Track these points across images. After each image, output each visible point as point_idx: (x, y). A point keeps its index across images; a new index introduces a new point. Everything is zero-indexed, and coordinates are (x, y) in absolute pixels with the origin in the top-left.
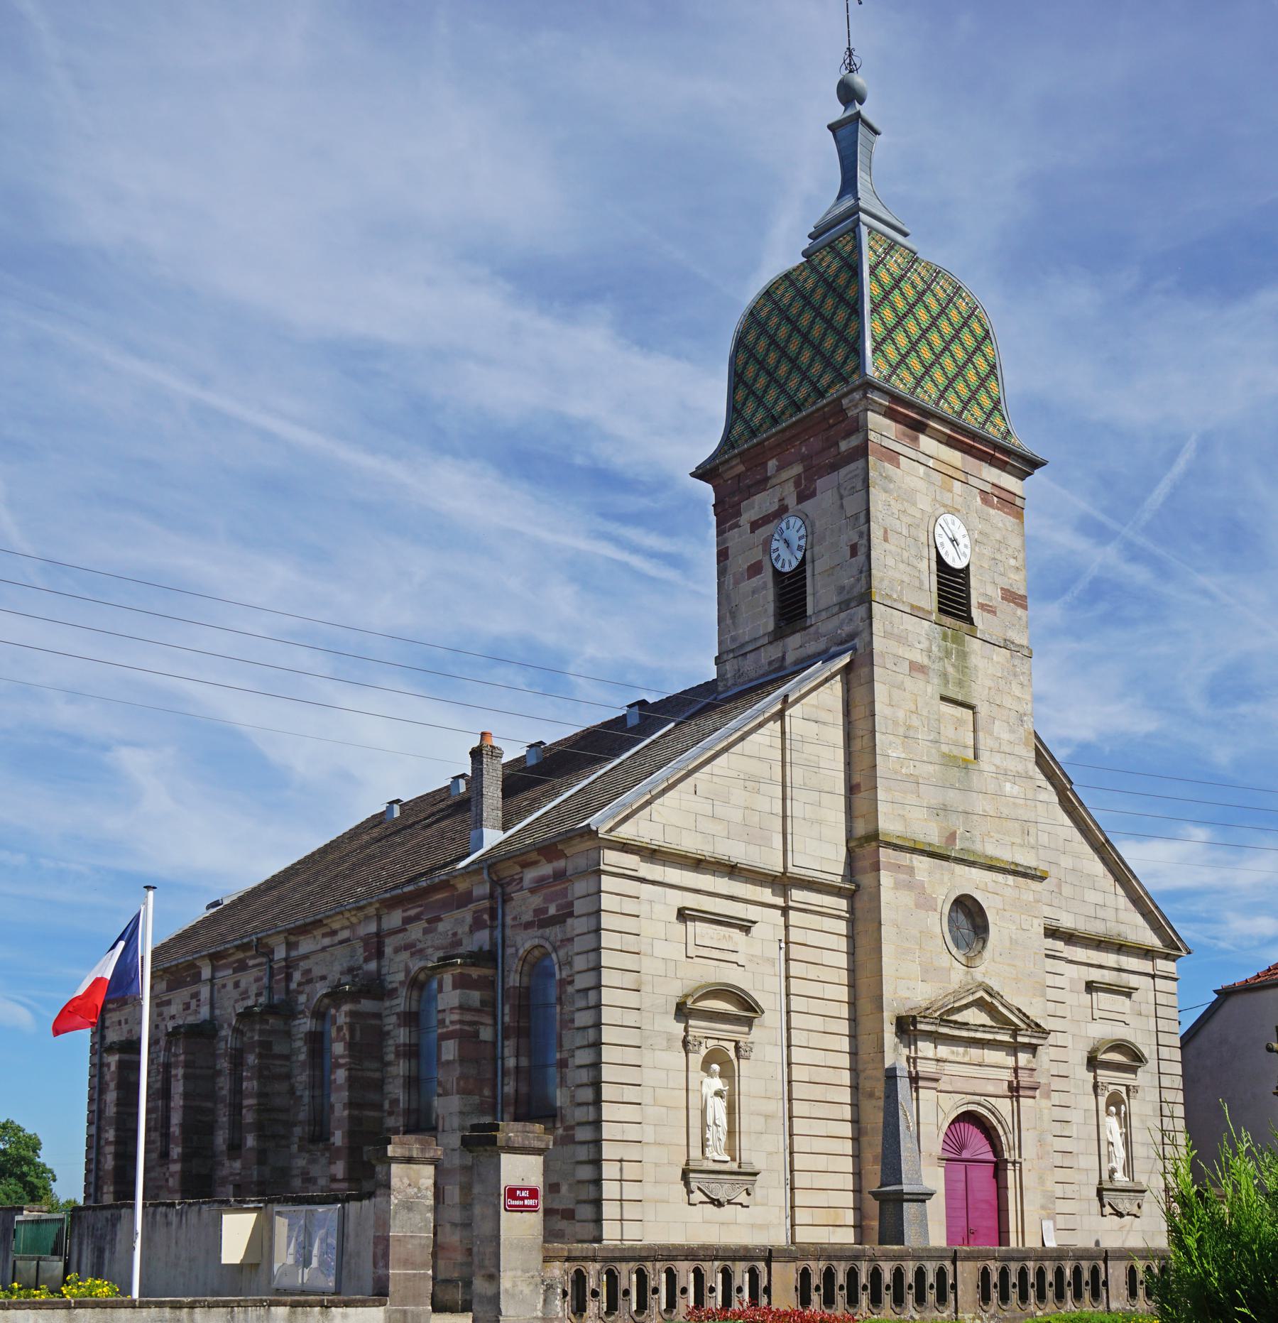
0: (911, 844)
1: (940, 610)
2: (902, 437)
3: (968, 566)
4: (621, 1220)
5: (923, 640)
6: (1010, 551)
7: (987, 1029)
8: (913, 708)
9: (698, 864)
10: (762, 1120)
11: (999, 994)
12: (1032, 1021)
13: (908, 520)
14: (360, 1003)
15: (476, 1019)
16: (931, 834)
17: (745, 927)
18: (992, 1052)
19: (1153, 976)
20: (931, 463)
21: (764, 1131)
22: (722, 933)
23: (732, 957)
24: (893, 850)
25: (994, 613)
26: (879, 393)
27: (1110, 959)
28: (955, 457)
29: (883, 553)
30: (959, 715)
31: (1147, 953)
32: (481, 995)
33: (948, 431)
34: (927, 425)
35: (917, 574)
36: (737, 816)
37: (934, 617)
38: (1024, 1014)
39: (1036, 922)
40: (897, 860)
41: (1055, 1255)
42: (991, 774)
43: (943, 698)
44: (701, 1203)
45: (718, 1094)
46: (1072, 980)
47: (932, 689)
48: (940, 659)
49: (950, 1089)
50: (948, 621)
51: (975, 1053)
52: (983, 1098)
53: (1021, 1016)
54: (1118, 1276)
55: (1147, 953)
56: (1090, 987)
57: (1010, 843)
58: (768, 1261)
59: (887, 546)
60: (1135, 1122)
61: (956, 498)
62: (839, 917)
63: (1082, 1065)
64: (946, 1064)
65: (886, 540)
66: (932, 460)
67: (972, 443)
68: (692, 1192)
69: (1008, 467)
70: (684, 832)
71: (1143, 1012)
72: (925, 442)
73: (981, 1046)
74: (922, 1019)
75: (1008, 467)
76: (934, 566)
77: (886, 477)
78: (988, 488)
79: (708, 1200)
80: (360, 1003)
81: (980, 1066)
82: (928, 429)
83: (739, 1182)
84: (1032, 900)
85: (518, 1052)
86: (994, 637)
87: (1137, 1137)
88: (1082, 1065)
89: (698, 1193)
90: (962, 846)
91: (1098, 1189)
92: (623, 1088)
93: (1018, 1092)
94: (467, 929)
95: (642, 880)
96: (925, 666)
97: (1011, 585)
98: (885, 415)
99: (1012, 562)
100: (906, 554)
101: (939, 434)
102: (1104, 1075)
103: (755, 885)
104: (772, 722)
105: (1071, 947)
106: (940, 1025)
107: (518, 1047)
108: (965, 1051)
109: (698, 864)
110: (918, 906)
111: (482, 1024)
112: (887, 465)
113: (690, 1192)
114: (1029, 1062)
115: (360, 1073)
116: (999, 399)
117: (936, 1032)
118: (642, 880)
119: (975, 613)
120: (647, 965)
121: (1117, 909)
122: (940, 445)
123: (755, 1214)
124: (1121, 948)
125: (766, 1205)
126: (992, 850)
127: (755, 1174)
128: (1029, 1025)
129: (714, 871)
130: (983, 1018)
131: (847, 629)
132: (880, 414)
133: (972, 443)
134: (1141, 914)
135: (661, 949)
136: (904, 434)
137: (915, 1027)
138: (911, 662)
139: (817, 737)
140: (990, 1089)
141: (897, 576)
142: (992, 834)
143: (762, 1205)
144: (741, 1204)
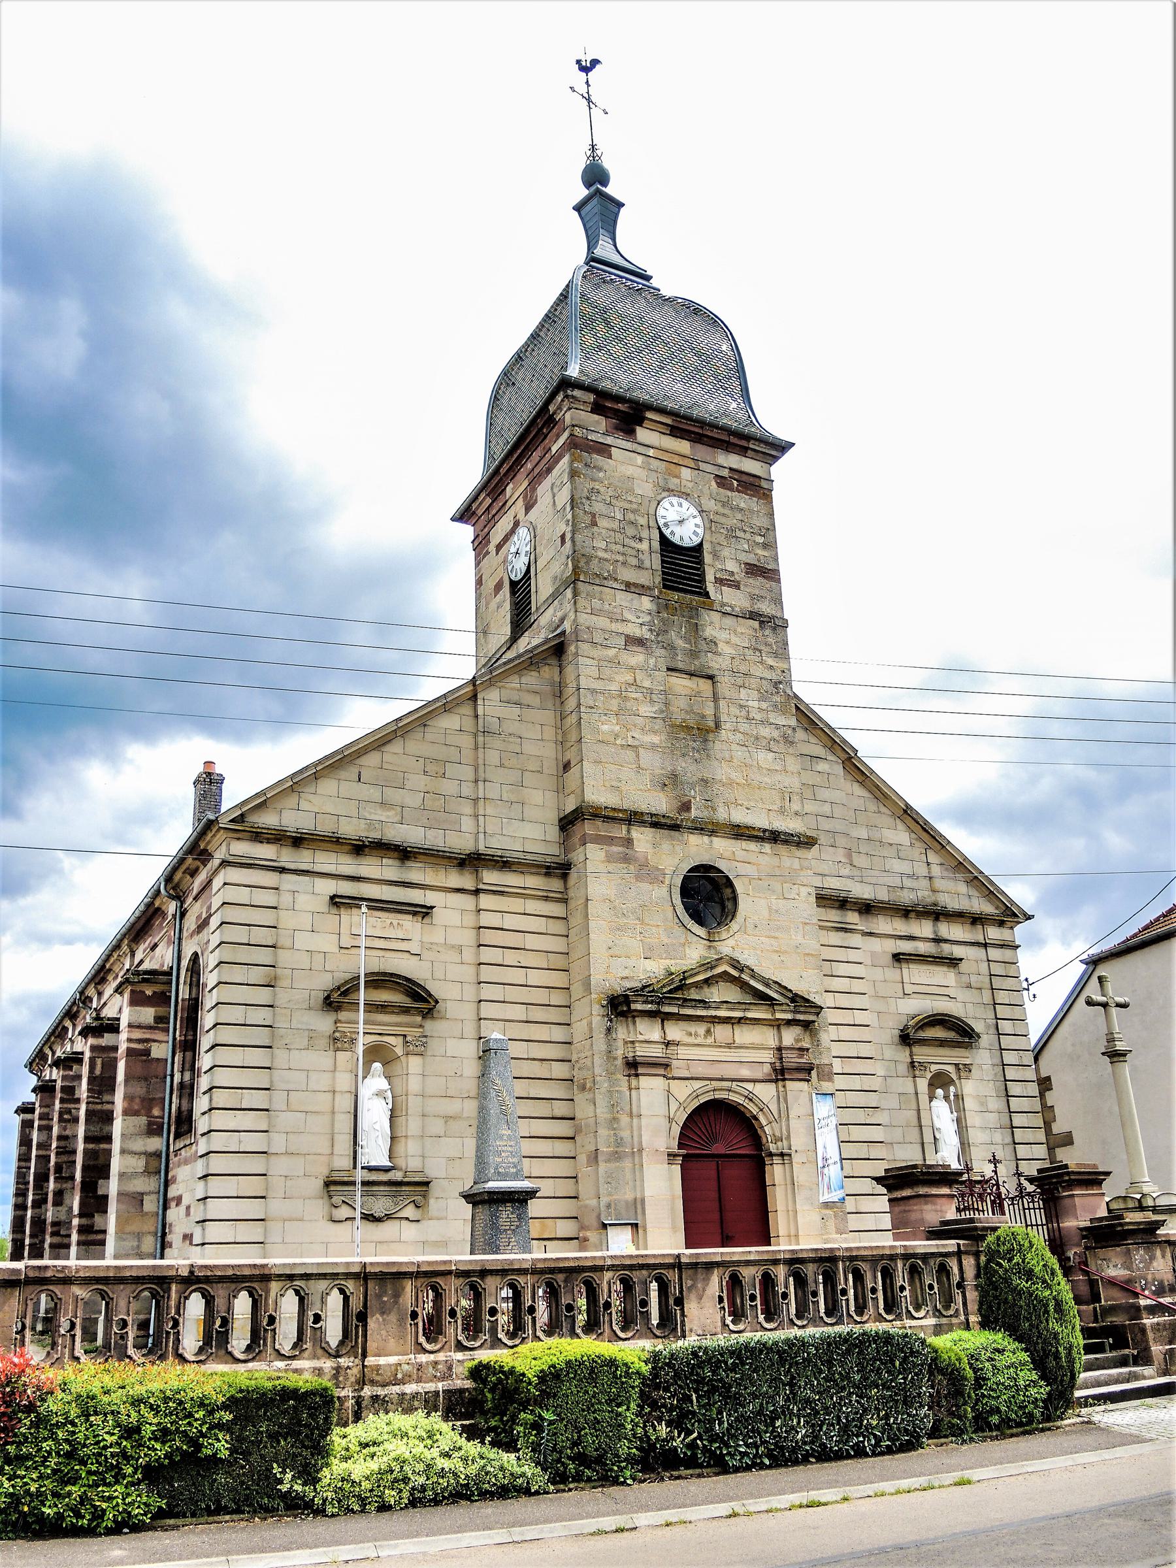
1: (665, 587)
3: (701, 545)
8: (632, 682)
10: (441, 1122)
14: (103, 1037)
15: (147, 1036)
16: (660, 803)
17: (423, 912)
19: (985, 945)
20: (651, 452)
21: (442, 1134)
28: (684, 446)
30: (695, 686)
31: (976, 920)
32: (156, 1011)
36: (413, 800)
37: (656, 592)
38: (785, 988)
39: (804, 891)
45: (379, 1094)
46: (873, 954)
49: (686, 1074)
55: (976, 920)
56: (898, 958)
60: (969, 1104)
61: (684, 482)
66: (652, 450)
69: (749, 452)
71: (973, 985)
75: (750, 453)
76: (656, 545)
78: (725, 473)
80: (103, 1037)
85: (183, 1068)
87: (973, 1119)
93: (783, 1074)
95: (283, 870)
102: (923, 1054)
107: (183, 1061)
111: (155, 1041)
114: (797, 1040)
115: (99, 1107)
118: (283, 870)
119: (710, 588)
120: (284, 958)
121: (930, 878)
123: (431, 1229)
124: (937, 914)
126: (739, 817)
127: (427, 1184)
131: (559, 614)
135: (304, 941)
137: (629, 1006)
138: (627, 636)
140: (745, 1073)
144: (407, 1219)
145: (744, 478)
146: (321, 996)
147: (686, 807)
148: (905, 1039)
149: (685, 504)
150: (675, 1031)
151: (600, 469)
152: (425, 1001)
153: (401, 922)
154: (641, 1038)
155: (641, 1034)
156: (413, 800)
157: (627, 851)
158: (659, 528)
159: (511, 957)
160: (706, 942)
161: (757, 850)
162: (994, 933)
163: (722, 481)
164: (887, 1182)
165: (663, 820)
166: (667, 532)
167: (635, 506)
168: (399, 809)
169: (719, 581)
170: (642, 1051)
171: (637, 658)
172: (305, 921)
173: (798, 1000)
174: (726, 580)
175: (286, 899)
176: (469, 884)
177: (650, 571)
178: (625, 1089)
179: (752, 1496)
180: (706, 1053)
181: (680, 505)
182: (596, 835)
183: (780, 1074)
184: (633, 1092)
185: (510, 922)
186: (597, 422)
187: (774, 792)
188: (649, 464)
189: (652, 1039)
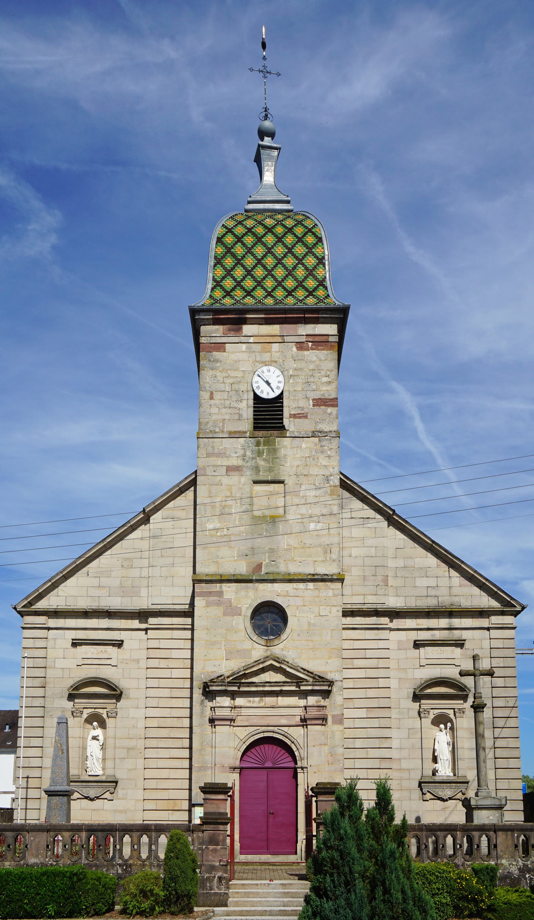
0: (219, 578)
2: (228, 332)
4: (26, 809)
5: (239, 450)
6: (323, 373)
7: (273, 684)
8: (228, 494)
9: (86, 614)
11: (285, 661)
12: (316, 675)
13: (231, 381)
17: (119, 644)
18: (285, 698)
20: (251, 340)
21: (126, 757)
22: (100, 650)
23: (108, 662)
24: (206, 583)
25: (306, 417)
26: (203, 313)
27: (443, 622)
28: (275, 329)
29: (209, 407)
33: (263, 316)
34: (246, 318)
35: (237, 411)
38: (308, 672)
39: (334, 609)
40: (209, 589)
41: (444, 828)
42: (296, 521)
43: (255, 482)
44: (430, 799)
47: (246, 478)
48: (253, 458)
50: (261, 433)
51: (269, 700)
52: (276, 728)
53: (306, 672)
54: (39, 842)
56: (417, 645)
58: (495, 832)
62: (185, 629)
63: (408, 697)
64: (242, 709)
65: (211, 398)
66: (252, 338)
67: (284, 316)
68: (425, 794)
70: (79, 598)
72: (247, 329)
73: (276, 695)
74: (212, 684)
76: (251, 402)
77: (213, 361)
78: (303, 339)
79: (83, 797)
81: (273, 708)
82: (248, 320)
83: (103, 787)
84: (332, 595)
86: (302, 433)
88: (408, 697)
89: (428, 794)
90: (267, 571)
91: (419, 782)
92: (30, 740)
95: (49, 629)
96: (240, 466)
97: (323, 395)
98: (214, 324)
99: (325, 379)
100: (227, 402)
101: (259, 320)
102: (426, 703)
104: (144, 525)
105: (400, 620)
106: (228, 686)
108: (260, 700)
109: (86, 614)
110: (225, 614)
113: (423, 794)
116: (325, 277)
117: (226, 690)
118: (49, 629)
120: (50, 673)
122: (260, 326)
126: (294, 569)
128: (314, 678)
129: (99, 616)
130: (280, 678)
132: (210, 325)
133: (284, 316)
134: (477, 587)
136: (230, 330)
139: (173, 527)
140: (284, 721)
141: (220, 417)
142: (295, 559)
143: (123, 799)
144: (107, 799)
145: (317, 339)
147: (259, 567)
148: (417, 697)
150: (240, 701)
152: (116, 690)
153: (106, 649)
154: (218, 705)
155: (218, 703)
156: (116, 583)
157: (219, 599)
158: (253, 391)
159: (163, 664)
160: (264, 647)
161: (303, 588)
163: (300, 346)
164: (49, 793)
165: (326, 577)
166: (258, 392)
167: (239, 379)
168: (108, 588)
169: (294, 416)
170: (219, 713)
171: (234, 479)
172: (60, 653)
173: (319, 679)
174: (298, 414)
175: (50, 644)
176: (144, 626)
178: (210, 733)
180: (259, 711)
182: (202, 592)
183: (304, 722)
184: (214, 735)
185: (164, 644)
186: (217, 329)
187: (319, 549)
188: (250, 348)
189: (224, 706)
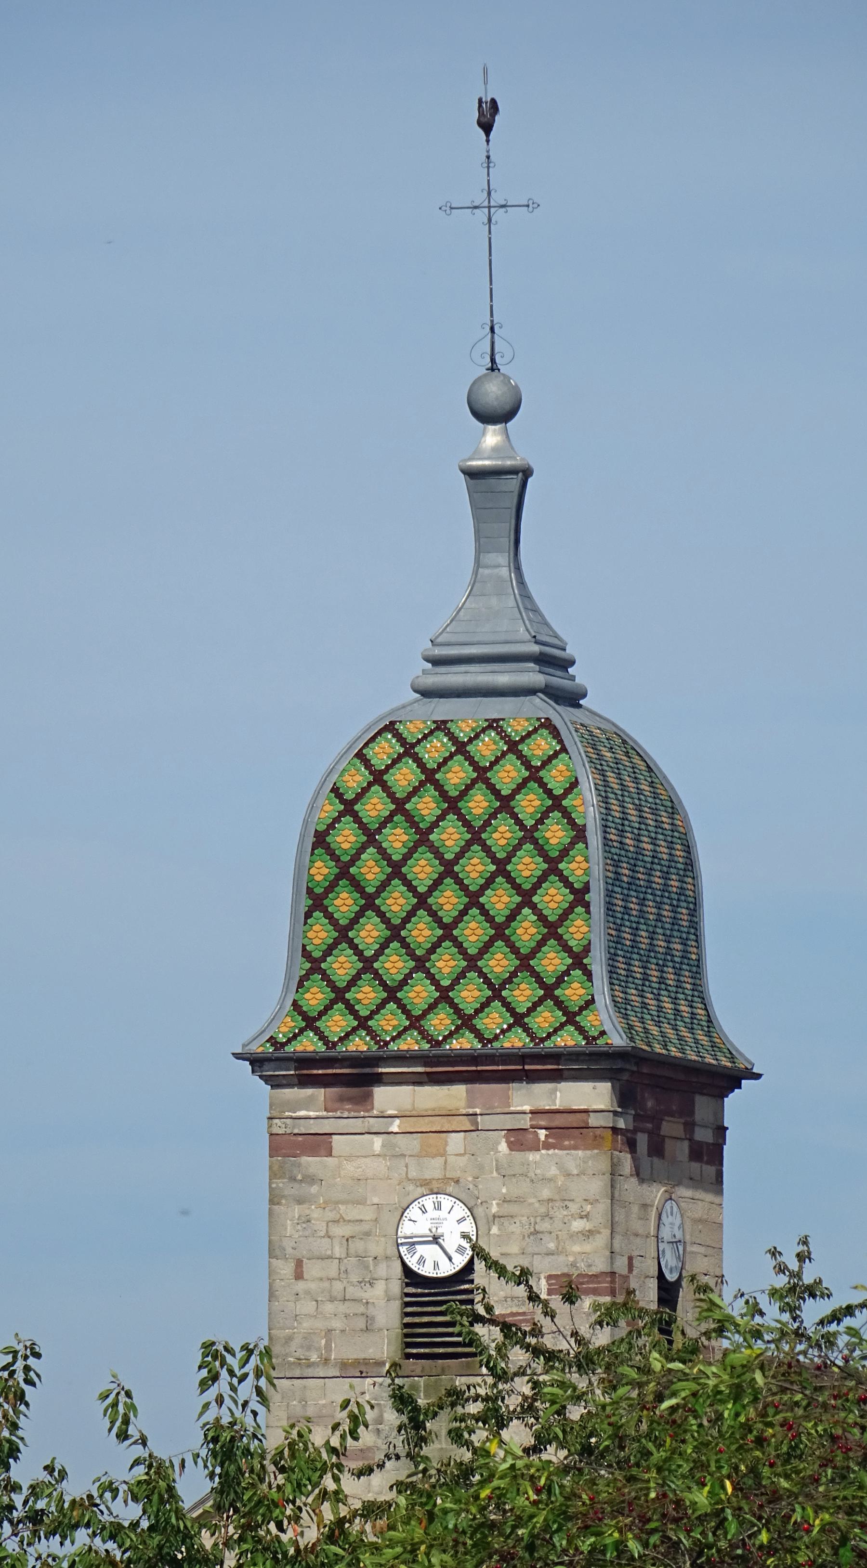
2: (337, 1105)
6: (574, 1208)
26: (272, 1064)
57: (36, 1556)
59: (301, 1286)
65: (299, 1275)
67: (474, 1068)
78: (526, 1122)
94: (606, 1436)
97: (573, 1265)
99: (578, 1225)
100: (338, 1286)
103: (508, 1083)
112: (305, 1160)
125: (271, 1256)
136: (342, 1099)
145: (559, 1121)
146: (437, 1419)
149: (447, 1202)
151: (311, 1180)
162: (628, 955)
167: (366, 1227)
177: (312, 1419)
179: (663, 1054)
181: (438, 1207)
